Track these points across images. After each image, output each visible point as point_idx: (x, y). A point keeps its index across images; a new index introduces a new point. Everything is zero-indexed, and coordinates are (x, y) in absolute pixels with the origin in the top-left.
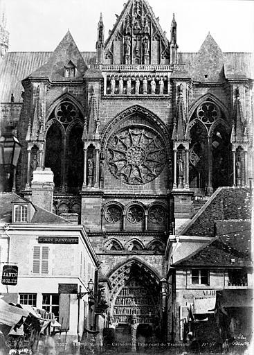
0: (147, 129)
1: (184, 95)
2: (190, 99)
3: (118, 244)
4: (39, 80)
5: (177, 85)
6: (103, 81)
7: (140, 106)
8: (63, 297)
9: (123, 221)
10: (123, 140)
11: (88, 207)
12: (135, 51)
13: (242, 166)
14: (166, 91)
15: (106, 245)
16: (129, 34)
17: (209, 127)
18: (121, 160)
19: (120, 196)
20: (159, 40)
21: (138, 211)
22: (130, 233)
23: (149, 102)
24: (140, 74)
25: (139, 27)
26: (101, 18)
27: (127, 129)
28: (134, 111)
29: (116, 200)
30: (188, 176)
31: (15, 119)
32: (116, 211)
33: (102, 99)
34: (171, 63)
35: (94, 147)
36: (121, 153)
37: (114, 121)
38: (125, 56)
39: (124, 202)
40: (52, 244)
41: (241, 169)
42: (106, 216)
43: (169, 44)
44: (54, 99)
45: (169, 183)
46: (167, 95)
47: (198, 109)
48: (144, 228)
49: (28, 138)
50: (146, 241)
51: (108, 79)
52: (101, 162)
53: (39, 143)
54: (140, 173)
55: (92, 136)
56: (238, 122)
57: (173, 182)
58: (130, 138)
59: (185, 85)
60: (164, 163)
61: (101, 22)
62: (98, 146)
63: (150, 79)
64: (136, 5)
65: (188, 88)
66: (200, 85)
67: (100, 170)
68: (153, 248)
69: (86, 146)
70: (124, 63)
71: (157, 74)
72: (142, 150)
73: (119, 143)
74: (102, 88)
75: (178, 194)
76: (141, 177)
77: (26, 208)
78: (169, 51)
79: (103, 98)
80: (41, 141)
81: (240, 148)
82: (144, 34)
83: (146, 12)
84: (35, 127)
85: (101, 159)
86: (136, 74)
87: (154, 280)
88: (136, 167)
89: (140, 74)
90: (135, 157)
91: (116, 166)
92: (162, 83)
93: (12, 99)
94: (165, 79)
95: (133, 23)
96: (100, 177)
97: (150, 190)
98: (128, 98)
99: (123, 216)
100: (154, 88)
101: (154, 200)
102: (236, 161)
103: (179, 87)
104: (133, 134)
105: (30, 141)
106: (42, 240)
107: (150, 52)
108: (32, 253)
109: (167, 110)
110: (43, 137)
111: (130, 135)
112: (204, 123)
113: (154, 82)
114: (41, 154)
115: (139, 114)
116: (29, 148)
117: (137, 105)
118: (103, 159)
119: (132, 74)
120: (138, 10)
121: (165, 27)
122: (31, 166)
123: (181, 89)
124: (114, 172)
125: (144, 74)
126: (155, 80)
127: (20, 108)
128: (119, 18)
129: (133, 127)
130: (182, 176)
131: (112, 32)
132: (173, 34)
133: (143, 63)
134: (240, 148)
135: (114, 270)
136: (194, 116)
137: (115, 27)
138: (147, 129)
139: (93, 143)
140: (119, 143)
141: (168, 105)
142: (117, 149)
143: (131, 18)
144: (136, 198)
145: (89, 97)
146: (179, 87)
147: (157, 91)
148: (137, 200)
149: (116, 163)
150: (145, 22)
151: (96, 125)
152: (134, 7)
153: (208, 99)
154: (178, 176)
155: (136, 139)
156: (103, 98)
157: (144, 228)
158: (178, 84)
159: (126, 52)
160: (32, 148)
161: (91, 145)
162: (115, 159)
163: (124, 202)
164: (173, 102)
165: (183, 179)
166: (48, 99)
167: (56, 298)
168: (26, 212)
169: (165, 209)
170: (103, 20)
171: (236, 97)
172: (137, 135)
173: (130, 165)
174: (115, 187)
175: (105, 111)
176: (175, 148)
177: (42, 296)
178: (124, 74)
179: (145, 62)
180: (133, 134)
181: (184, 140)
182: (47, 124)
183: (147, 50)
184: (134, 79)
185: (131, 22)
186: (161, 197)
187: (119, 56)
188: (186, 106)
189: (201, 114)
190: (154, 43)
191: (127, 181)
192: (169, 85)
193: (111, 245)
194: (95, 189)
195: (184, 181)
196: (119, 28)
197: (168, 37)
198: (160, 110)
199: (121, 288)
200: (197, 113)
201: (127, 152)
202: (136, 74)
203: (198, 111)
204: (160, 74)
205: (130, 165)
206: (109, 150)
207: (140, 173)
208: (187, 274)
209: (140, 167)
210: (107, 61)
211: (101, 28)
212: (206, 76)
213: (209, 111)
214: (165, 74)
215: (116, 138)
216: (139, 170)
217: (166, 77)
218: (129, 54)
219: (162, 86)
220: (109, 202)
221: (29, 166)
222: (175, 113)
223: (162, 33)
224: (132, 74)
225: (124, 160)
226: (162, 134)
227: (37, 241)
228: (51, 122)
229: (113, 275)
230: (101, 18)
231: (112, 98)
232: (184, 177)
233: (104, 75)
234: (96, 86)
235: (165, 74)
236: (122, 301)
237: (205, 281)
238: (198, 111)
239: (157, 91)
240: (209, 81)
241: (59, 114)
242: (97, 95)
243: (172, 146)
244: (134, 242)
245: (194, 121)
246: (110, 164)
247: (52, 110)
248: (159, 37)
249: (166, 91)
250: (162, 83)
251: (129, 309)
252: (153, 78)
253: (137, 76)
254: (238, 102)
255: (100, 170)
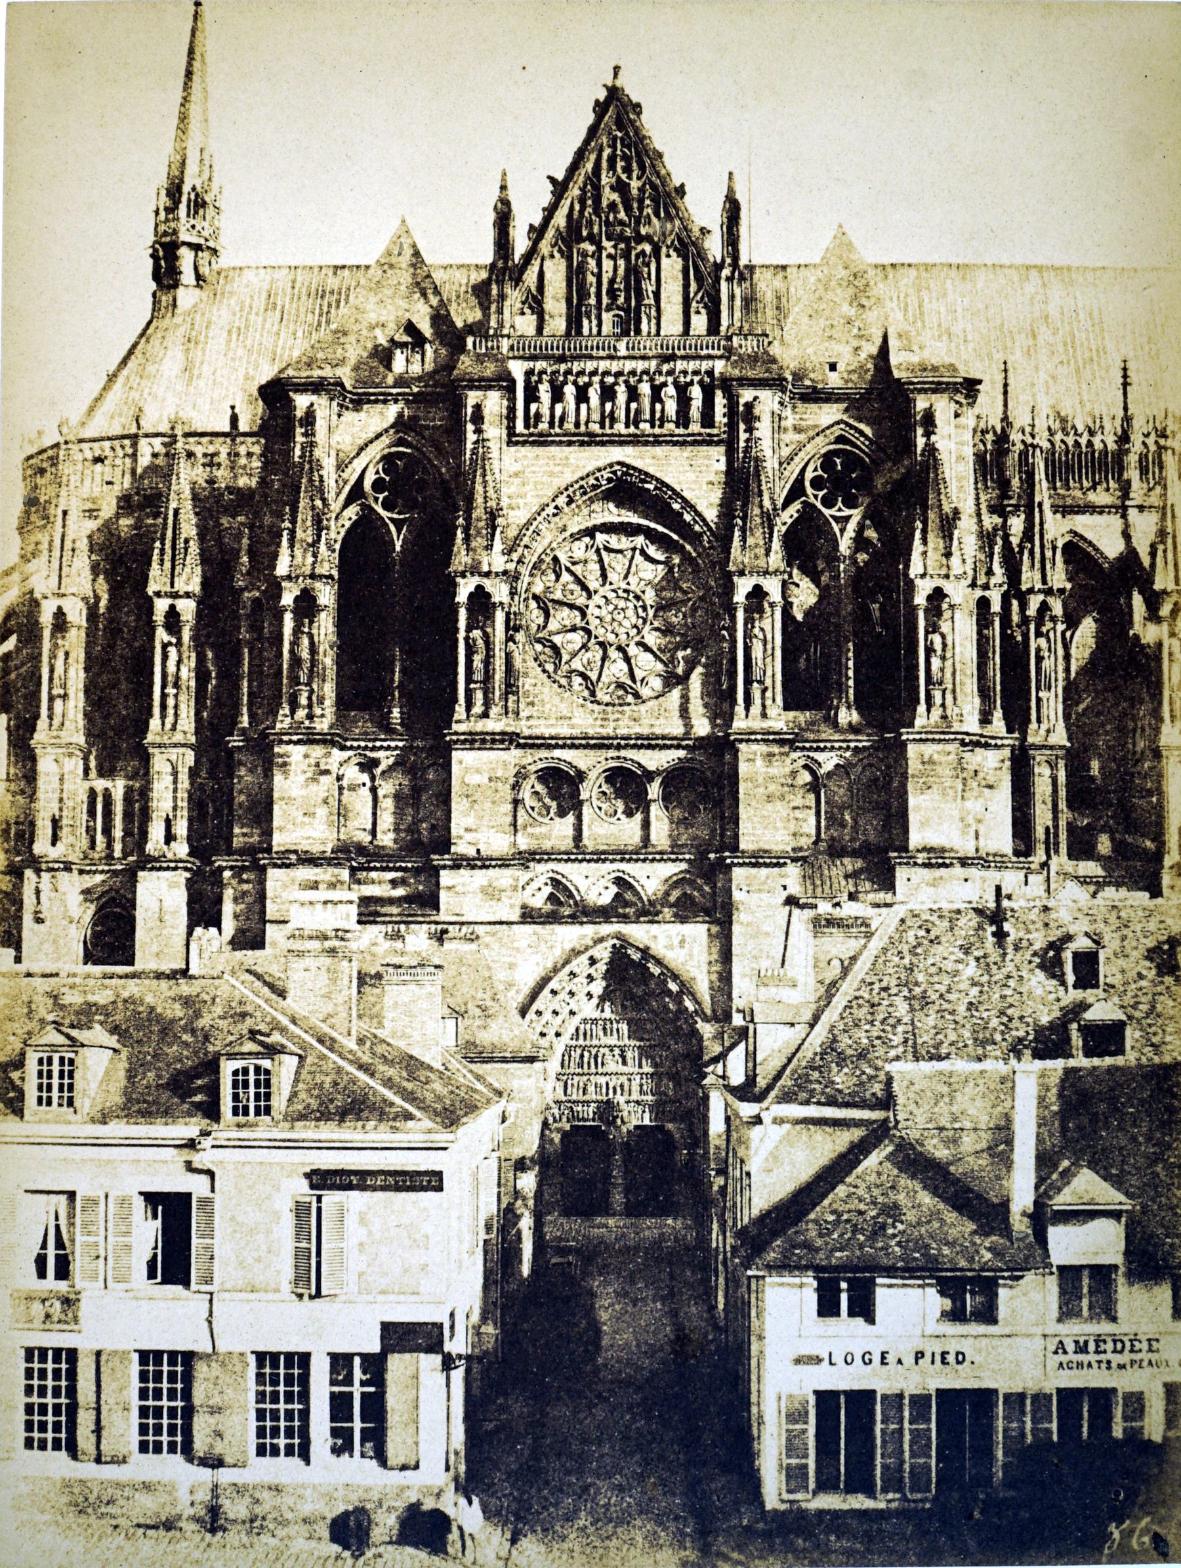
0: (650, 534)
1: (763, 429)
2: (791, 440)
3: (566, 888)
4: (316, 387)
5: (742, 401)
6: (511, 389)
7: (628, 466)
8: (397, 1364)
9: (579, 818)
10: (578, 569)
11: (474, 779)
12: (612, 293)
13: (944, 645)
14: (707, 418)
15: (530, 889)
16: (591, 238)
17: (848, 527)
18: (574, 629)
19: (572, 743)
20: (685, 258)
21: (628, 786)
22: (600, 856)
23: (658, 450)
24: (629, 365)
25: (622, 215)
26: (503, 188)
27: (590, 532)
28: (609, 480)
29: (557, 753)
30: (779, 677)
31: (242, 482)
32: (562, 787)
33: (510, 443)
34: (723, 329)
35: (489, 596)
36: (572, 607)
37: (549, 510)
38: (580, 305)
39: (580, 759)
40: (355, 1194)
41: (943, 658)
42: (529, 801)
43: (719, 267)
44: (361, 442)
45: (721, 702)
46: (715, 431)
47: (811, 468)
48: (646, 839)
49: (282, 569)
50: (652, 879)
51: (527, 382)
52: (510, 639)
53: (318, 585)
54: (631, 670)
55: (480, 566)
56: (932, 515)
57: (734, 702)
58: (601, 561)
59: (767, 401)
60: (700, 622)
61: (505, 202)
62: (499, 591)
63: (659, 380)
64: (614, 147)
65: (776, 407)
66: (816, 396)
67: (509, 657)
68: (672, 899)
69: (465, 589)
70: (579, 333)
71: (680, 365)
72: (637, 598)
73: (566, 577)
74: (512, 410)
75: (749, 736)
76: (634, 681)
77: (267, 1072)
78: (719, 291)
79: (512, 439)
80: (321, 577)
81: (938, 595)
82: (640, 239)
83: (642, 167)
84: (305, 534)
85: (512, 628)
86: (615, 366)
87: (678, 998)
88: (620, 648)
89: (629, 365)
90: (617, 620)
91: (556, 650)
92: (696, 392)
93: (234, 419)
94: (707, 380)
95: (605, 203)
96: (509, 685)
97: (668, 716)
98: (591, 440)
99: (581, 803)
100: (671, 407)
101: (682, 753)
102: (927, 633)
103: (749, 406)
104: (609, 550)
105: (289, 578)
106: (322, 1180)
107: (657, 295)
108: (288, 1221)
109: (713, 478)
110: (329, 564)
111: (598, 551)
112: (827, 512)
113: (671, 390)
114: (323, 615)
115: (626, 488)
116: (287, 599)
117: (619, 463)
118: (517, 629)
119: (603, 365)
120: (620, 164)
121: (703, 211)
122: (292, 652)
123: (756, 412)
124: (550, 667)
125: (640, 366)
126: (676, 384)
127: (257, 449)
128: (560, 188)
129: (608, 528)
130: (761, 682)
131: (537, 233)
132: (730, 229)
133: (638, 332)
134: (938, 595)
135: (556, 970)
136: (797, 490)
137: (550, 212)
138: (650, 534)
139: (488, 584)
140: (566, 577)
141: (714, 460)
142: (558, 595)
143: (597, 188)
144: (619, 747)
145: (471, 437)
146: (749, 406)
147: (683, 418)
148: (623, 753)
149: (557, 640)
150: (641, 201)
151: (494, 528)
152: (607, 152)
153: (840, 439)
154: (748, 682)
155: (617, 564)
156: (512, 439)
157: (646, 839)
158: (746, 395)
159: (583, 294)
160: (297, 599)
161: (479, 588)
162: (553, 625)
163: (580, 759)
164: (730, 445)
165: (764, 691)
166: (350, 442)
167: (375, 1365)
168: (268, 1084)
169: (705, 783)
170: (512, 196)
171: (928, 434)
172: (620, 551)
173: (602, 645)
174: (552, 709)
175: (524, 479)
176: (740, 597)
177: (328, 1359)
178: (576, 367)
179: (644, 327)
180: (609, 550)
181: (766, 573)
182: (342, 520)
183: (649, 287)
184: (610, 380)
185: (597, 199)
186: (702, 743)
187: (562, 307)
188: (771, 464)
189: (817, 483)
190: (672, 265)
191: (593, 694)
192: (720, 400)
193: (548, 890)
194: (494, 725)
195: (769, 694)
196: (560, 219)
197: (714, 248)
198: (694, 477)
199: (576, 1021)
200: (807, 484)
201: (591, 603)
202: (615, 366)
203: (809, 475)
204: (692, 366)
205: (602, 645)
206: (536, 597)
207: (631, 670)
208: (801, 1286)
209: (633, 650)
210: (526, 324)
211: (503, 219)
212: (833, 367)
213: (842, 474)
214: (705, 365)
215: (556, 559)
216: (627, 660)
217: (710, 373)
218: (592, 301)
219: (697, 403)
220: (536, 760)
221: (286, 655)
222: (740, 482)
223: (696, 232)
224: (603, 365)
225: (583, 629)
226: (699, 563)
227: (305, 1183)
228: (352, 512)
229: (553, 985)
230: (503, 188)
231: (542, 441)
232: (768, 682)
233: (517, 369)
234: (494, 403)
235: (705, 365)
236: (582, 1056)
237: (864, 1308)
238: (809, 475)
239: (683, 418)
240: (840, 384)
241: (378, 485)
242: (494, 431)
243: (729, 589)
244: (619, 881)
245: (796, 506)
246: (539, 641)
247: (356, 476)
248: (688, 247)
249: (707, 418)
250: (696, 392)
251: (602, 1080)
252: (670, 379)
253: (619, 374)
254: (931, 450)
255: (509, 657)
